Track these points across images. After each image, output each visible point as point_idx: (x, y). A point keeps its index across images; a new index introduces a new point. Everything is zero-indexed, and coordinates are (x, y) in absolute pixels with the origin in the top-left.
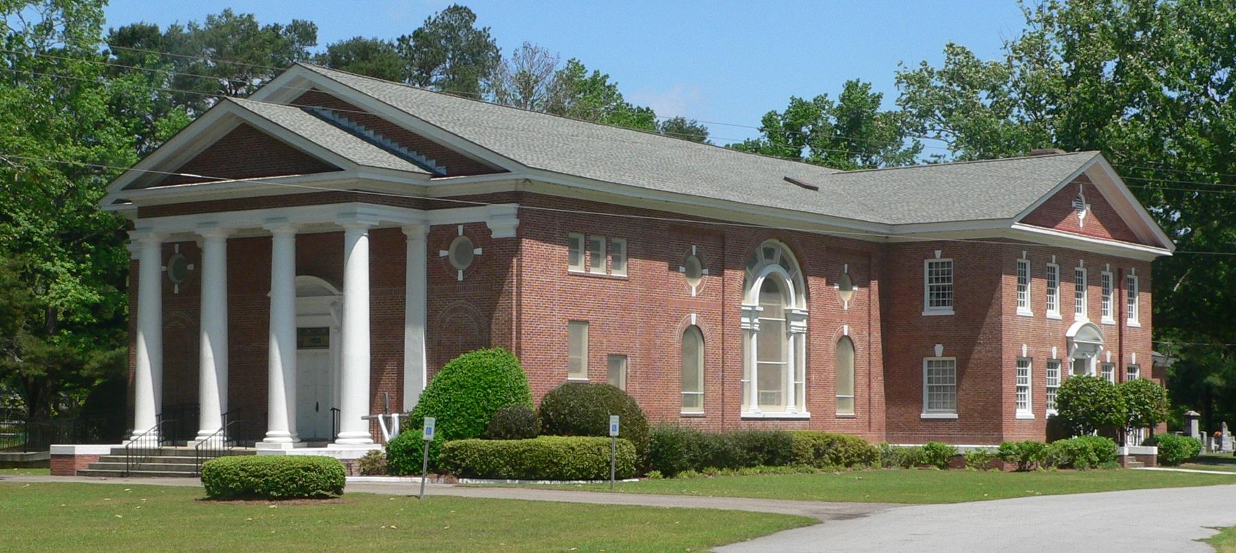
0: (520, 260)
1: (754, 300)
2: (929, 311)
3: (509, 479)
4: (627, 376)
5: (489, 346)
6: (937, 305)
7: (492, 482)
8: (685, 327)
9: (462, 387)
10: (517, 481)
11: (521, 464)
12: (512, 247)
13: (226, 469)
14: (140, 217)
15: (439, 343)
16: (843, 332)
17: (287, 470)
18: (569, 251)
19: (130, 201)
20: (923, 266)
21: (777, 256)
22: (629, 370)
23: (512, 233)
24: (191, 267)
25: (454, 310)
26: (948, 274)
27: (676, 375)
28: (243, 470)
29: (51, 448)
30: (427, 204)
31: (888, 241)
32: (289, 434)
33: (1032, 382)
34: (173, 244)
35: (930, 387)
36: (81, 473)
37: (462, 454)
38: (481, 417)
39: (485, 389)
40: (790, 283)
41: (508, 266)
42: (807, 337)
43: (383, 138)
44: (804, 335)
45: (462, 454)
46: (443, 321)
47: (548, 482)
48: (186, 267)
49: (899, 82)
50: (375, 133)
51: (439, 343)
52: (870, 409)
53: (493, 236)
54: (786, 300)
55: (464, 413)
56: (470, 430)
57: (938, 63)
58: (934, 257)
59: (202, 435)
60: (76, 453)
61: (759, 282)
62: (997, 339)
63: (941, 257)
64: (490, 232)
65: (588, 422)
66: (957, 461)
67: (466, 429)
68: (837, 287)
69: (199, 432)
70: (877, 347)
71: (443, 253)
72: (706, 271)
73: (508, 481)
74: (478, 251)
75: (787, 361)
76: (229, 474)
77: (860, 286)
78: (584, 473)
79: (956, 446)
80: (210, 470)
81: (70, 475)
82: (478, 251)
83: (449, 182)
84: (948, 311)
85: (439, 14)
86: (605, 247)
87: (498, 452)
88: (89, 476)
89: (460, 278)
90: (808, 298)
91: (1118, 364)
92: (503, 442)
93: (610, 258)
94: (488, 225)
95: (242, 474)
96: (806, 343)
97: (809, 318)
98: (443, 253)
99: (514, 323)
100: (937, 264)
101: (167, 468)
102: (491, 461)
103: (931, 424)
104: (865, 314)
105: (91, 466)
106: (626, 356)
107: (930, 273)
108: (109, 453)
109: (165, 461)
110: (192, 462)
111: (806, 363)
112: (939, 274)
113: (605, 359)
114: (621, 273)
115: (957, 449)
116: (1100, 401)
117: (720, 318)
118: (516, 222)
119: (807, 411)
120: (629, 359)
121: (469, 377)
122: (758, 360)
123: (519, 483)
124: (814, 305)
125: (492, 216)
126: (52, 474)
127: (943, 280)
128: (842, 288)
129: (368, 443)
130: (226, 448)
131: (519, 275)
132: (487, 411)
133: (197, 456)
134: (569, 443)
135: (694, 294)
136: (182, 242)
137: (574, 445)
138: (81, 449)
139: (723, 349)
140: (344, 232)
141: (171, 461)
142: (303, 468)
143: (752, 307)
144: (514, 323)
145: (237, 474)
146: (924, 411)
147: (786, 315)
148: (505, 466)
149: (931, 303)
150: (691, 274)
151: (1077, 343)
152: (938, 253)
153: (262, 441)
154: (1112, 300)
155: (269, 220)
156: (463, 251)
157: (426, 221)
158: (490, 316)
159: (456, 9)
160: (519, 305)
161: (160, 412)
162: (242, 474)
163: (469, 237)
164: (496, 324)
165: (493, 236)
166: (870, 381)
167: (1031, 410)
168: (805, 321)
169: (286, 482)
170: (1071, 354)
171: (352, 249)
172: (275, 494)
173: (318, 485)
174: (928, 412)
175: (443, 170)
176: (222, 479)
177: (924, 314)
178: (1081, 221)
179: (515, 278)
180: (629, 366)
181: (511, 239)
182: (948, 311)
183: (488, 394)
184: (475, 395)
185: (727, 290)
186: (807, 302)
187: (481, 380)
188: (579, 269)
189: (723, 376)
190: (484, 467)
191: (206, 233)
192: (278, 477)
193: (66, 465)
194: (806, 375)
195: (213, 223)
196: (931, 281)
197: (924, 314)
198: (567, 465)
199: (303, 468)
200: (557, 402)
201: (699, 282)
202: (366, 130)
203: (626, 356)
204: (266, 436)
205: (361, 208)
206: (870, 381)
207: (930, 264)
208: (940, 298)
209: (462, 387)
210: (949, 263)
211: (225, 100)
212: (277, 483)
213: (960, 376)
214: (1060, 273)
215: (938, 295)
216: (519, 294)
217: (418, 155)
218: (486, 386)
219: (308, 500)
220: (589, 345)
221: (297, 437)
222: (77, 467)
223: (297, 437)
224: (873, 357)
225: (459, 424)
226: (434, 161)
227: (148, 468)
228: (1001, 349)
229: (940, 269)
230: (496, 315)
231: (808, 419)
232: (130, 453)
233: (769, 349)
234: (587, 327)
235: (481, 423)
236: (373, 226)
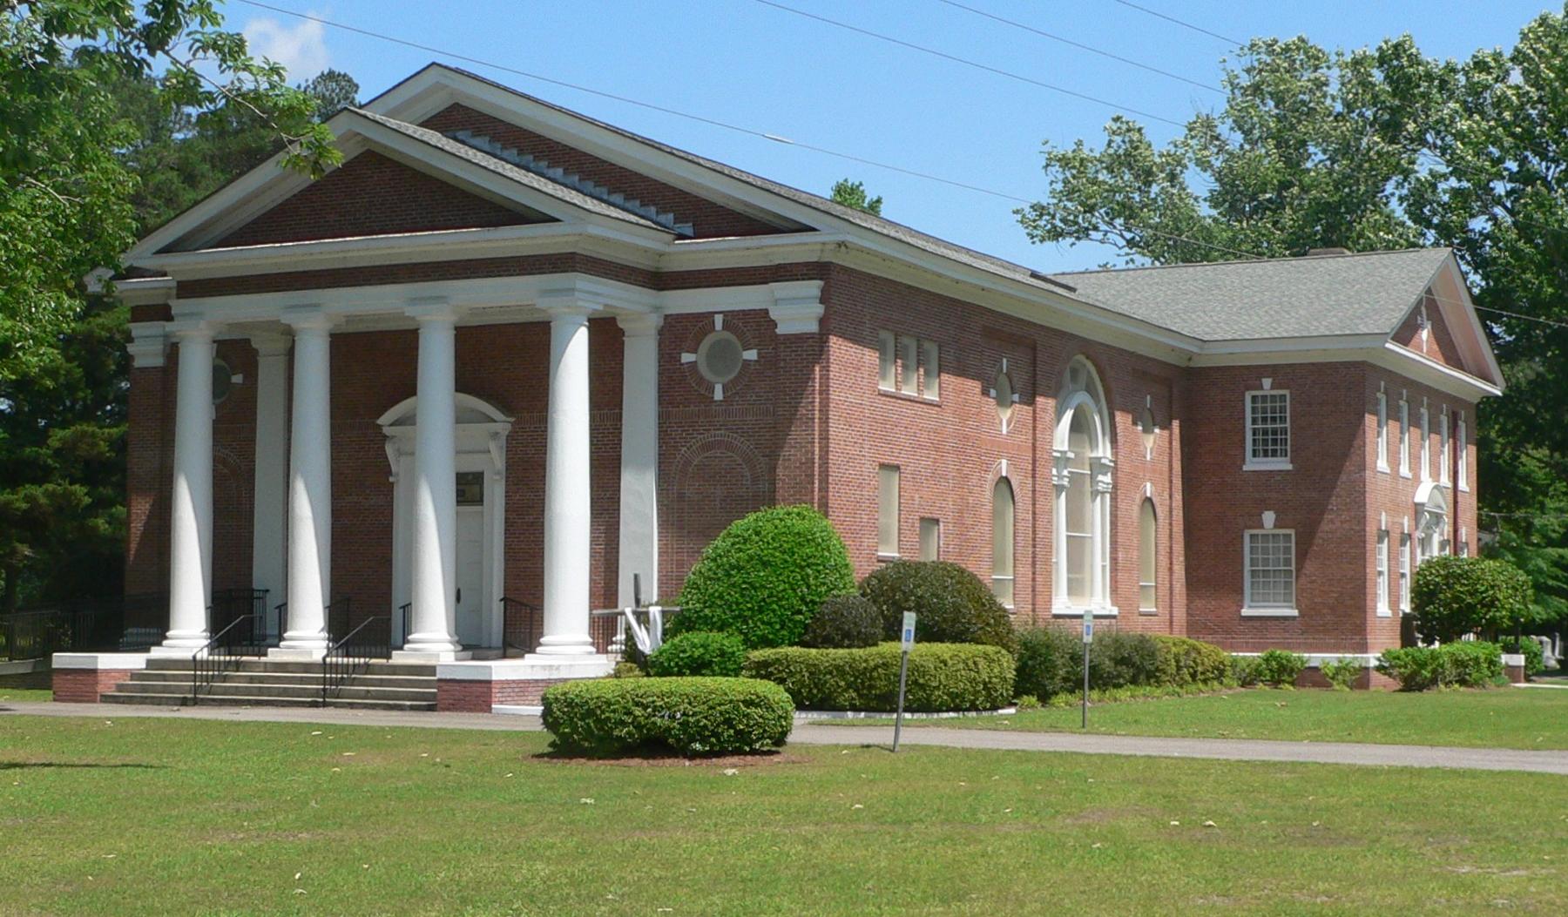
0: (826, 369)
1: (1063, 442)
2: (1252, 464)
3: (850, 710)
4: (939, 551)
5: (772, 502)
6: (1272, 456)
7: (824, 716)
8: (997, 478)
9: (765, 564)
10: (862, 714)
11: (871, 687)
12: (812, 348)
13: (609, 703)
14: (179, 297)
15: (681, 497)
16: (1145, 491)
17: (720, 705)
18: (880, 358)
20: (1243, 400)
21: (1083, 379)
22: (941, 543)
23: (813, 327)
24: (237, 379)
25: (707, 447)
26: (1281, 412)
27: (986, 551)
28: (637, 704)
29: (54, 659)
30: (660, 280)
31: (1192, 364)
32: (449, 638)
33: (1389, 566)
35: (1252, 571)
36: (107, 699)
37: (780, 672)
38: (800, 612)
39: (802, 568)
40: (1097, 419)
41: (809, 377)
42: (1111, 498)
43: (580, 180)
44: (1108, 496)
45: (780, 672)
46: (687, 463)
47: (924, 716)
48: (230, 379)
49: (1048, 165)
50: (566, 172)
51: (681, 497)
52: (1171, 602)
54: (1091, 447)
55: (775, 606)
56: (785, 632)
57: (1096, 145)
58: (1261, 387)
59: (291, 639)
60: (494, 678)
61: (1068, 416)
62: (1360, 504)
63: (1272, 388)
65: (945, 620)
66: (1314, 678)
67: (778, 630)
68: (1140, 428)
69: (542, 640)
70: (1178, 514)
71: (687, 358)
72: (1016, 397)
73: (849, 713)
74: (751, 355)
75: (1092, 532)
76: (614, 711)
77: (1162, 428)
78: (957, 701)
79: (1306, 655)
80: (570, 704)
81: (88, 702)
82: (751, 355)
83: (708, 247)
84: (1282, 464)
85: (310, 82)
86: (915, 353)
87: (837, 667)
88: (123, 703)
89: (718, 395)
90: (1114, 441)
91: (1452, 541)
92: (841, 652)
93: (922, 371)
94: (771, 314)
95: (638, 712)
96: (1111, 506)
97: (1115, 471)
98: (687, 358)
99: (817, 465)
100: (1264, 398)
101: (261, 691)
102: (826, 682)
103: (1258, 624)
104: (1166, 469)
105: (120, 688)
106: (937, 521)
107: (1254, 410)
108: (144, 666)
109: (251, 679)
110: (186, 678)
111: (1111, 537)
112: (1268, 413)
113: (917, 525)
114: (931, 395)
115: (1309, 659)
116: (1482, 593)
117: (1030, 467)
118: (819, 309)
119: (1113, 605)
120: (941, 524)
121: (775, 549)
122: (1068, 530)
123: (866, 717)
124: (1122, 450)
125: (776, 301)
126: (55, 700)
127: (1274, 420)
128: (1145, 431)
129: (590, 653)
130: (211, 658)
131: (825, 391)
132: (806, 604)
133: (325, 673)
134: (939, 653)
135: (1005, 431)
137: (946, 657)
138: (107, 661)
139: (1034, 513)
140: (549, 322)
141: (261, 680)
142: (744, 702)
143: (1061, 452)
144: (817, 465)
145: (629, 713)
146: (1246, 606)
147: (1091, 465)
148: (846, 690)
149: (1255, 454)
150: (1002, 402)
151: (1429, 512)
152: (1267, 382)
154: (1446, 453)
155: (414, 301)
156: (721, 354)
157: (657, 309)
158: (773, 455)
159: (331, 76)
160: (825, 437)
161: (328, 604)
162: (638, 712)
163: (735, 333)
164: (785, 468)
165: (780, 330)
166: (1171, 564)
167: (1387, 604)
168: (1109, 474)
169: (718, 725)
170: (1421, 527)
171: (567, 346)
172: (698, 746)
173: (765, 731)
174: (1250, 607)
175: (688, 229)
176: (598, 721)
177: (1245, 468)
178: (1425, 344)
179: (817, 396)
180: (942, 535)
181: (810, 336)
182: (1282, 464)
183: (808, 575)
184: (788, 577)
185: (1039, 427)
186: (1112, 448)
187: (793, 554)
188: (887, 386)
189: (1034, 552)
190: (815, 691)
191: (298, 321)
192: (706, 718)
193: (83, 685)
194: (1111, 553)
195: (315, 306)
196: (1254, 421)
197: (1245, 468)
198: (937, 688)
199: (743, 702)
200: (893, 589)
201: (1009, 412)
202: (548, 167)
203: (937, 521)
204: (166, 638)
205: (582, 282)
206: (1171, 564)
207: (1254, 398)
208: (1269, 444)
209: (765, 564)
210: (1283, 397)
211: (345, 112)
212: (705, 726)
213: (1302, 555)
214: (1409, 414)
215: (1265, 442)
216: (825, 420)
217: (642, 206)
218: (803, 564)
219: (749, 758)
220: (900, 503)
221: (458, 642)
222: (101, 689)
223: (458, 642)
224: (1175, 529)
225: (770, 624)
226: (671, 216)
227: (226, 691)
228: (1365, 517)
229: (1269, 405)
230: (785, 453)
231: (1114, 617)
232: (198, 667)
233: (1076, 519)
234: (897, 475)
235: (800, 621)
236: (596, 310)
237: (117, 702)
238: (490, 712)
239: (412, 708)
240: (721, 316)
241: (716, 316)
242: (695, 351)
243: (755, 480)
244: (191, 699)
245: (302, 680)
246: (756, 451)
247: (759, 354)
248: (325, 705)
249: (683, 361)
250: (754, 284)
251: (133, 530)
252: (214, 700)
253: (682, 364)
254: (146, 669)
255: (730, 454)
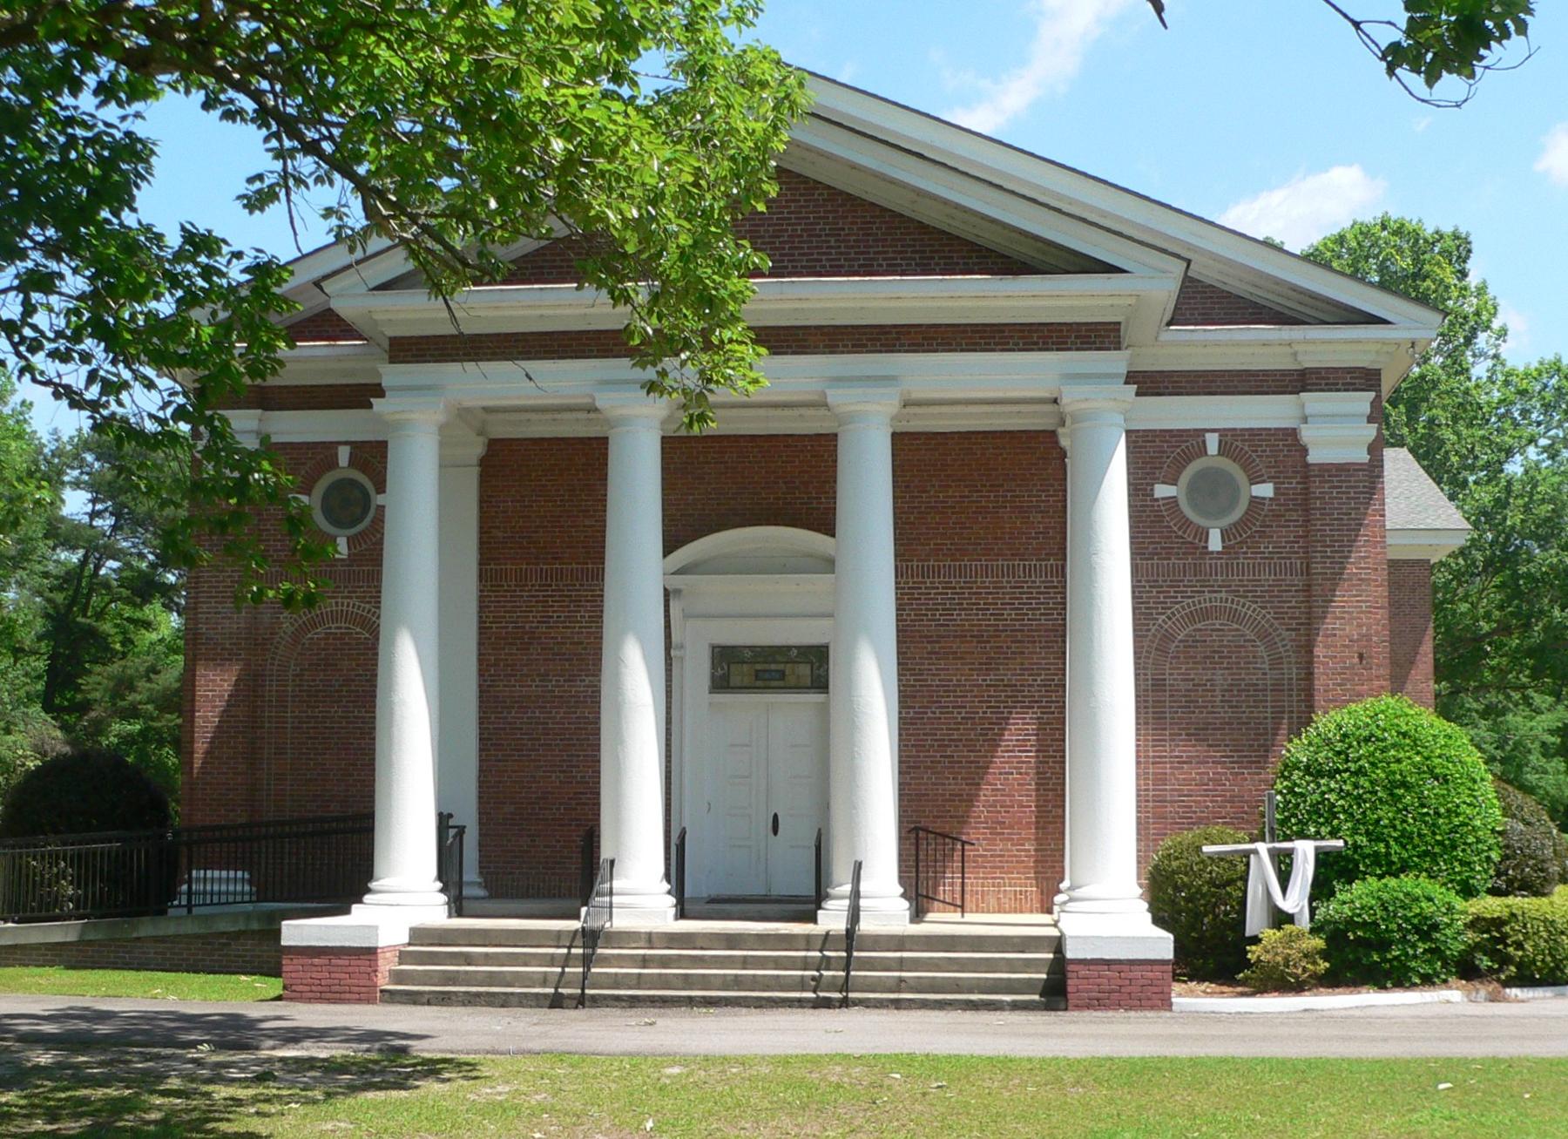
14: (393, 360)
19: (360, 338)
34: (334, 445)
36: (391, 997)
53: (1311, 459)
60: (380, 945)
64: (1304, 451)
69: (373, 885)
71: (1162, 491)
82: (1265, 490)
88: (429, 1003)
89: (1215, 543)
136: (1225, 430)
153: (360, 901)
155: (838, 380)
156: (1211, 489)
165: (1311, 459)
204: (369, 891)
230: (1329, 624)
237: (415, 1003)
238: (1171, 1010)
239: (1015, 1006)
240: (1216, 435)
241: (1208, 435)
242: (1174, 482)
243: (1276, 662)
244: (570, 997)
245: (777, 963)
246: (1276, 622)
247: (1276, 489)
248: (845, 1003)
249: (1157, 495)
250: (1198, 394)
251: (199, 722)
252: (618, 998)
253: (1157, 500)
254: (409, 944)
255: (1235, 626)
